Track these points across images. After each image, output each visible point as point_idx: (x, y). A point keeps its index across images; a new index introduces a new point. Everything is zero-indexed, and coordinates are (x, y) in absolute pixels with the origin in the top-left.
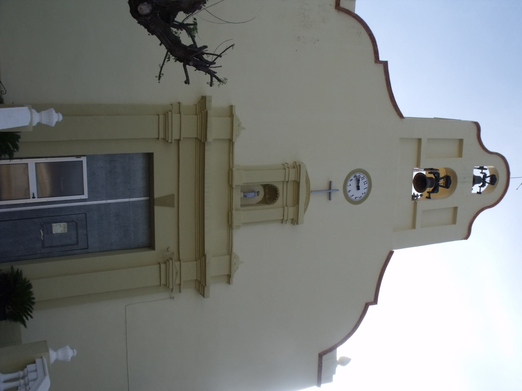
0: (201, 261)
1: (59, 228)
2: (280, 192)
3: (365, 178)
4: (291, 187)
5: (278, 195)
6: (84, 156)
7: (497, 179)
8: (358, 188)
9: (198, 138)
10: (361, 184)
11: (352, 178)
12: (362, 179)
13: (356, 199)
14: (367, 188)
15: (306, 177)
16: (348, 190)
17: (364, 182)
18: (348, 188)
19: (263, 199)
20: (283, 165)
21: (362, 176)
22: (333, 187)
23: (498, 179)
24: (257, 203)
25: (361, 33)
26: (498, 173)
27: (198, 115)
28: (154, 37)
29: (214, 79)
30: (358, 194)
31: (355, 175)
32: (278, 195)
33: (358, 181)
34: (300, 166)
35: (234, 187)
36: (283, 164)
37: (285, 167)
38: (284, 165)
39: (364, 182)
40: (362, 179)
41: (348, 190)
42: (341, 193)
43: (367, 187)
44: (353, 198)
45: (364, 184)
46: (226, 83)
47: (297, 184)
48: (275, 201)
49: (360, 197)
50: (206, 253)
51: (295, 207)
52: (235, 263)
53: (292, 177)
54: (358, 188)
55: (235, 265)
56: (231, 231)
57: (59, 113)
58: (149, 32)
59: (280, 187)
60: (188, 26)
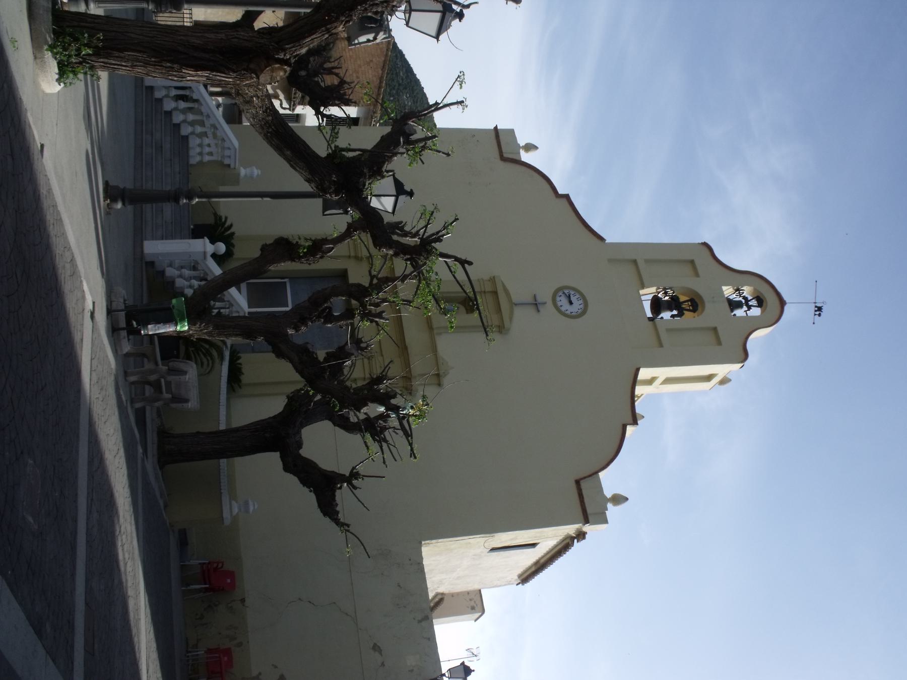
1: (229, 581)
6: (287, 278)
7: (763, 299)
8: (571, 303)
10: (573, 299)
11: (560, 293)
18: (559, 304)
21: (572, 292)
23: (764, 297)
26: (760, 292)
28: (260, 252)
30: (577, 306)
33: (569, 297)
43: (441, 290)
46: (435, 204)
50: (407, 345)
54: (571, 303)
57: (205, 238)
58: (244, 281)
60: (214, 314)
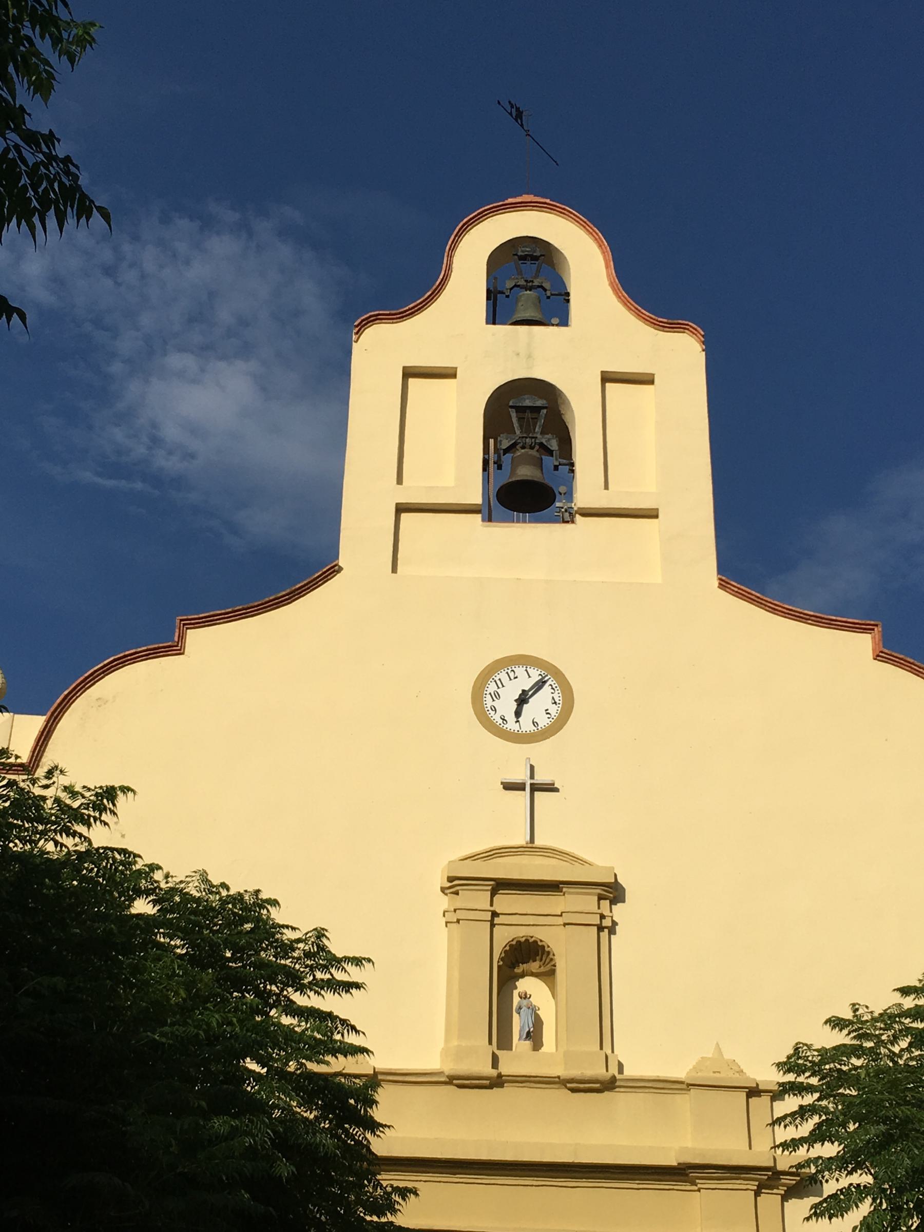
0: (383, 1164)
2: (521, 933)
3: (498, 677)
4: (506, 902)
5: (529, 938)
9: (755, 1188)
12: (500, 685)
13: (558, 702)
14: (528, 669)
15: (475, 860)
16: (532, 728)
17: (510, 679)
19: (541, 980)
20: (448, 924)
22: (521, 775)
24: (553, 996)
25: (99, 699)
27: (699, 1186)
29: (509, 111)
31: (489, 709)
32: (531, 940)
34: (451, 879)
35: (494, 1073)
36: (446, 926)
37: (454, 919)
38: (447, 923)
39: (510, 679)
40: (500, 685)
41: (532, 728)
42: (538, 752)
43: (525, 668)
44: (554, 710)
45: (516, 678)
47: (500, 886)
48: (547, 949)
49: (552, 688)
51: (564, 890)
52: (714, 1072)
53: (480, 899)
55: (719, 1072)
56: (622, 1084)
59: (504, 936)
